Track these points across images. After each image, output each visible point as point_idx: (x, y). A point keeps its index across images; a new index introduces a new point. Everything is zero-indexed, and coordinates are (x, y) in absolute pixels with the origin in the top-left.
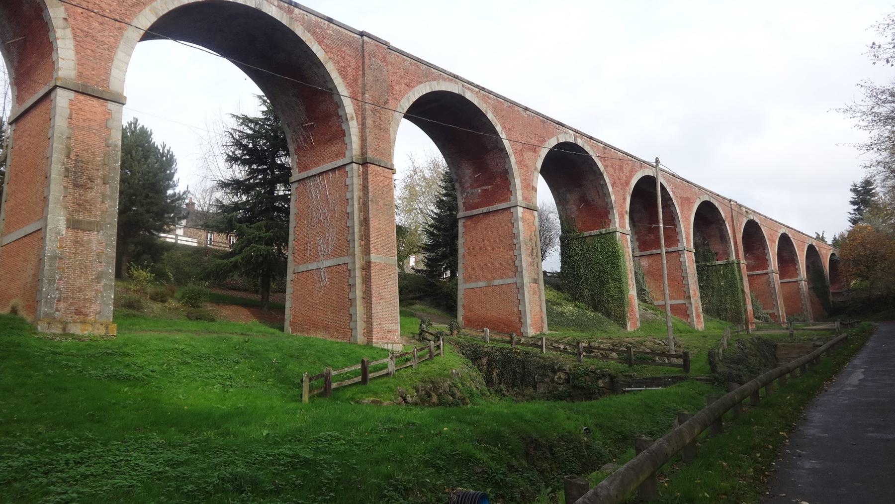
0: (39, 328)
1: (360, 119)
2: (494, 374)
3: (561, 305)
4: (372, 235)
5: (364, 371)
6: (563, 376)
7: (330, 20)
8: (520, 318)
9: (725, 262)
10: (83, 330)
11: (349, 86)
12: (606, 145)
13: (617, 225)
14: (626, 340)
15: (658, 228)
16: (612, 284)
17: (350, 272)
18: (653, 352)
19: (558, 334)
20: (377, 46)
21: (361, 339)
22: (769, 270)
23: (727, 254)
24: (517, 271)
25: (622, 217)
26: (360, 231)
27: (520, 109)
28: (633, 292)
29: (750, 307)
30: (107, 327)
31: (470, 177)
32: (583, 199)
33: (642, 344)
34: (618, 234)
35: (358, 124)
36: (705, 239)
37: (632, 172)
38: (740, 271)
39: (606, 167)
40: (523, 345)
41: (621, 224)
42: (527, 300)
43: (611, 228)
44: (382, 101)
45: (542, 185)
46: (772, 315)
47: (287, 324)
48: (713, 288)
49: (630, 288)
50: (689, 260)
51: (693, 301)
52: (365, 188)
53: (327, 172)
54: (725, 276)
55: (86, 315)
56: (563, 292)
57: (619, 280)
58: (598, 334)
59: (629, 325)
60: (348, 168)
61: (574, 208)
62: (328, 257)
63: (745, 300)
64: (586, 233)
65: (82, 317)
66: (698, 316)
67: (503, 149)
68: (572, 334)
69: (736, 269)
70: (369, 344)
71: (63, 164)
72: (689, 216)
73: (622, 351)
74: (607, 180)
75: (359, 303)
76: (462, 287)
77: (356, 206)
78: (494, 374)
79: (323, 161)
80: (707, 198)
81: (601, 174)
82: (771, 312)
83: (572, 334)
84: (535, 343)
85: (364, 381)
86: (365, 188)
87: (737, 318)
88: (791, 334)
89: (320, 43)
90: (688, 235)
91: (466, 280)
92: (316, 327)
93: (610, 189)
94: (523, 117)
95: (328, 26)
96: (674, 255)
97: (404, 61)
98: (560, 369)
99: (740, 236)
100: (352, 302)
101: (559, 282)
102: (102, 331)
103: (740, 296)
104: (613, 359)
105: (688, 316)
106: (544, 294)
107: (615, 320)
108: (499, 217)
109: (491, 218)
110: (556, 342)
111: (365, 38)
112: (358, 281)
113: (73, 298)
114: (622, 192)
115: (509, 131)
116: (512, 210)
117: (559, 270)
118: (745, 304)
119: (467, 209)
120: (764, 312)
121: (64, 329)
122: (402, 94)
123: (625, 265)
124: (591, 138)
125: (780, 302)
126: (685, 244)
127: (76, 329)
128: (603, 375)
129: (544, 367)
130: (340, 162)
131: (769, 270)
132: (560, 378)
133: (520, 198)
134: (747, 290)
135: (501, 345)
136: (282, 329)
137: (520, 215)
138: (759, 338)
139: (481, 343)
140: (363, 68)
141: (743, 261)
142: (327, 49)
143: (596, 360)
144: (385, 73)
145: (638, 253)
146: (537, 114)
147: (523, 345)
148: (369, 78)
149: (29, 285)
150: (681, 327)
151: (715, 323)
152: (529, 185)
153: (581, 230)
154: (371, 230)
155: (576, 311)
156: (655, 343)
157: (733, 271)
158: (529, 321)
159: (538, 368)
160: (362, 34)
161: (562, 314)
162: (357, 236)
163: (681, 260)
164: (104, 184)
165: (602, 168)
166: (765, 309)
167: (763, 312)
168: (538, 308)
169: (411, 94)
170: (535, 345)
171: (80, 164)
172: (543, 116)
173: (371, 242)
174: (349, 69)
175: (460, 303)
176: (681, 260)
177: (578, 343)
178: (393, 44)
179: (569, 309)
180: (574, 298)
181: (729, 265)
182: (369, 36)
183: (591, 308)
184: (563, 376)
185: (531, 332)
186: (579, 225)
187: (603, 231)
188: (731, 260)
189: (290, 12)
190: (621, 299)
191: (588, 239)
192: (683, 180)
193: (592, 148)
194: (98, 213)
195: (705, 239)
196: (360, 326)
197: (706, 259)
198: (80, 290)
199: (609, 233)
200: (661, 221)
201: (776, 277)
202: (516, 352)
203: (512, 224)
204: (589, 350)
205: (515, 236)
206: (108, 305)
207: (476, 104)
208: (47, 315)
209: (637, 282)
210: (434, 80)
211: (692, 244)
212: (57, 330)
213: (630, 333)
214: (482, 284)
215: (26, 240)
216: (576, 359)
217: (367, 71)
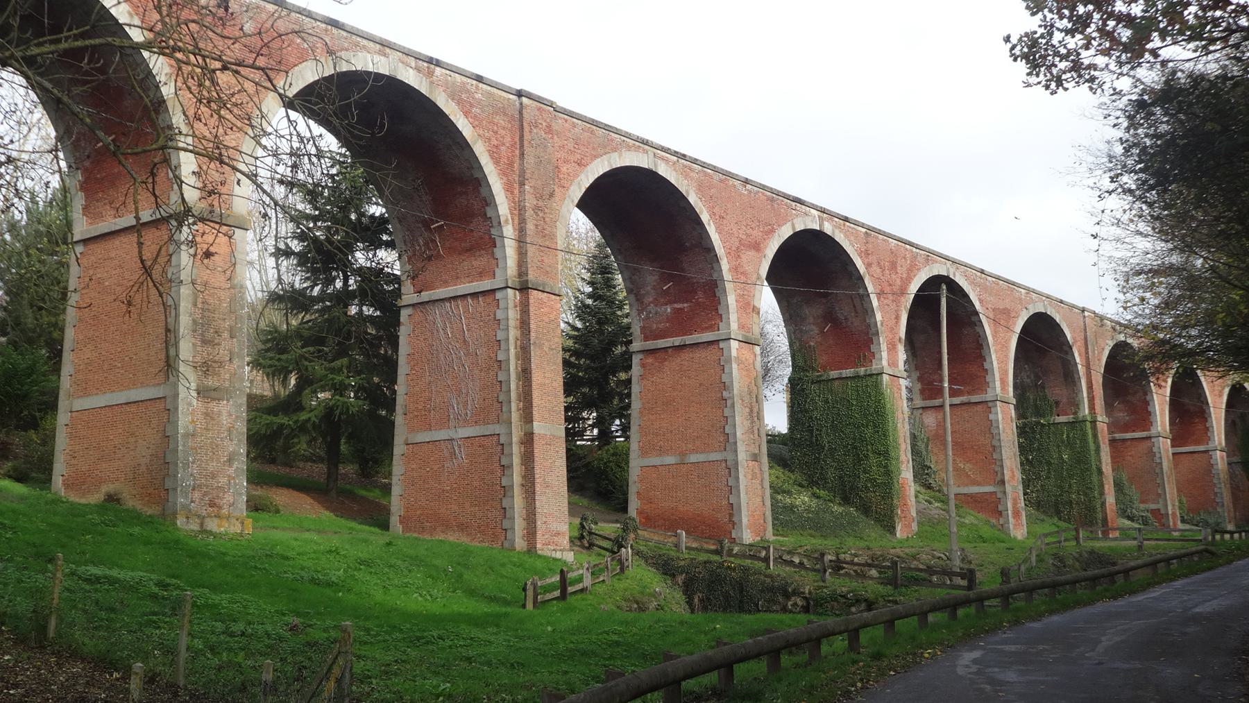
0: (178, 523)
1: (516, 221)
2: (696, 600)
3: (789, 493)
4: (536, 394)
5: (564, 583)
6: (800, 602)
7: (479, 79)
8: (731, 515)
9: (1070, 418)
10: (220, 526)
11: (503, 173)
12: (870, 229)
13: (885, 363)
14: (892, 551)
15: (950, 382)
16: (873, 460)
17: (503, 448)
18: (930, 570)
19: (789, 541)
20: (539, 109)
21: (520, 544)
22: (1153, 432)
23: (1075, 404)
24: (728, 442)
25: (892, 348)
26: (518, 387)
27: (737, 183)
28: (906, 474)
29: (1110, 499)
30: (242, 523)
31: (654, 288)
32: (830, 317)
33: (914, 557)
34: (885, 377)
35: (514, 229)
36: (1038, 377)
37: (912, 270)
38: (1095, 436)
39: (868, 266)
40: (736, 556)
41: (891, 358)
42: (742, 488)
43: (875, 367)
44: (546, 192)
45: (767, 300)
46: (1156, 513)
47: (394, 520)
48: (1049, 464)
49: (903, 467)
50: (1005, 419)
51: (1008, 488)
52: (524, 325)
53: (464, 296)
54: (1070, 444)
55: (220, 508)
56: (792, 472)
57: (885, 454)
58: (850, 541)
59: (899, 528)
60: (499, 295)
61: (815, 330)
62: (466, 423)
63: (1102, 486)
64: (834, 374)
65: (215, 509)
66: (1017, 514)
67: (710, 249)
68: (812, 542)
69: (1090, 431)
70: (531, 549)
71: (191, 315)
72: (1008, 341)
73: (884, 567)
74: (870, 288)
75: (517, 490)
76: (636, 465)
77: (512, 351)
78: (696, 600)
79: (457, 279)
80: (1040, 308)
81: (861, 278)
82: (1153, 506)
83: (812, 542)
84: (756, 552)
85: (564, 596)
86: (524, 325)
87: (1090, 516)
88: (1140, 547)
89: (466, 114)
90: (1004, 373)
91: (644, 453)
92: (447, 526)
93: (875, 303)
94: (741, 195)
95: (477, 87)
96: (979, 407)
97: (574, 126)
98: (796, 593)
99: (1098, 380)
100: (506, 491)
101: (787, 456)
102: (236, 528)
103: (1095, 478)
104: (871, 578)
105: (1000, 513)
106: (766, 470)
107: (877, 520)
108: (699, 354)
109: (686, 355)
110: (789, 553)
111: (524, 100)
112: (516, 461)
113: (207, 486)
114: (893, 306)
115: (720, 219)
116: (722, 345)
117: (784, 430)
118: (1102, 493)
119: (646, 339)
120: (1142, 506)
121: (202, 525)
122: (572, 177)
123: (895, 429)
124: (846, 219)
125: (1171, 491)
126: (998, 390)
127: (212, 525)
128: (857, 601)
129: (771, 589)
130: (486, 285)
131: (1153, 432)
132: (795, 604)
133: (734, 326)
134: (1107, 468)
135: (703, 557)
136: (385, 526)
137: (734, 353)
138: (1092, 552)
139: (673, 553)
140: (522, 146)
141: (1102, 418)
142: (476, 123)
143: (847, 580)
144: (550, 150)
145: (919, 402)
146: (763, 187)
147: (736, 556)
148: (530, 160)
149: (143, 468)
150: (986, 531)
151: (1048, 526)
152: (748, 304)
153: (824, 368)
154: (534, 387)
155: (814, 503)
156: (933, 556)
157: (1085, 435)
158: (745, 520)
159: (762, 591)
160: (520, 94)
161: (791, 508)
162: (513, 395)
163: (991, 417)
164: (232, 337)
165: (862, 269)
166: (1142, 502)
167: (1141, 508)
168: (759, 499)
169: (582, 176)
170: (753, 557)
171: (206, 314)
172: (772, 191)
173: (534, 405)
174: (503, 148)
175: (633, 490)
176: (991, 417)
177: (823, 555)
178: (562, 103)
179: (803, 499)
180: (813, 481)
181: (1077, 424)
182: (530, 96)
183: (838, 500)
184: (800, 602)
185: (748, 537)
186: (823, 359)
187: (862, 371)
188: (1081, 415)
189: (430, 74)
190: (887, 485)
191: (836, 383)
192: (999, 278)
193: (846, 236)
194: (227, 376)
195: (1038, 377)
196: (519, 525)
197: (1039, 413)
198: (213, 476)
199: (871, 375)
200: (946, 379)
201: (1165, 446)
202: (729, 567)
203: (722, 366)
204: (837, 566)
205: (725, 386)
206: (241, 494)
207: (673, 181)
208: (184, 507)
209: (915, 451)
210: (614, 150)
211: (1011, 389)
212: (194, 526)
213: (900, 542)
214: (670, 460)
215: (133, 408)
216: (818, 578)
217: (527, 150)
